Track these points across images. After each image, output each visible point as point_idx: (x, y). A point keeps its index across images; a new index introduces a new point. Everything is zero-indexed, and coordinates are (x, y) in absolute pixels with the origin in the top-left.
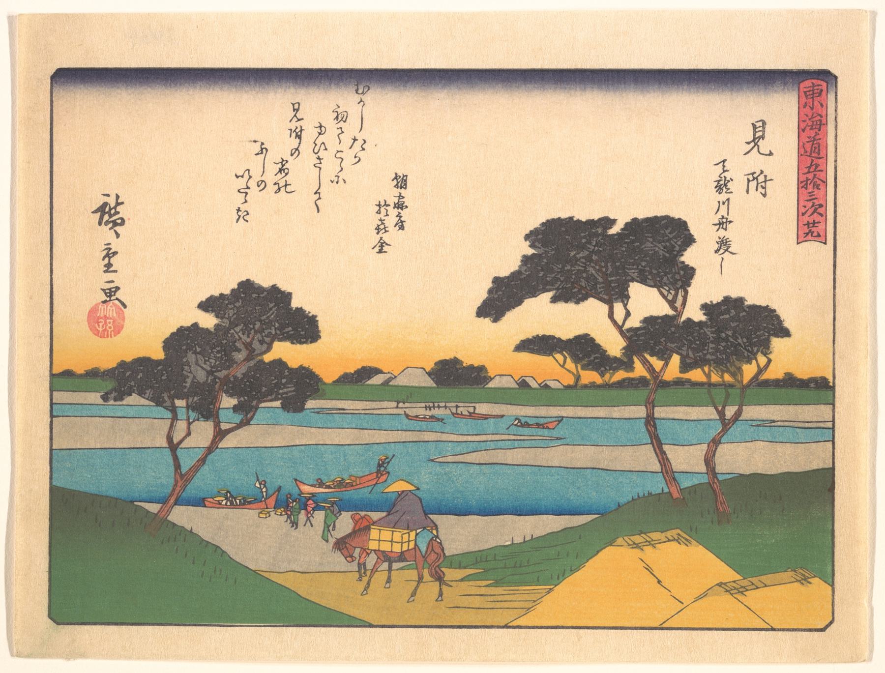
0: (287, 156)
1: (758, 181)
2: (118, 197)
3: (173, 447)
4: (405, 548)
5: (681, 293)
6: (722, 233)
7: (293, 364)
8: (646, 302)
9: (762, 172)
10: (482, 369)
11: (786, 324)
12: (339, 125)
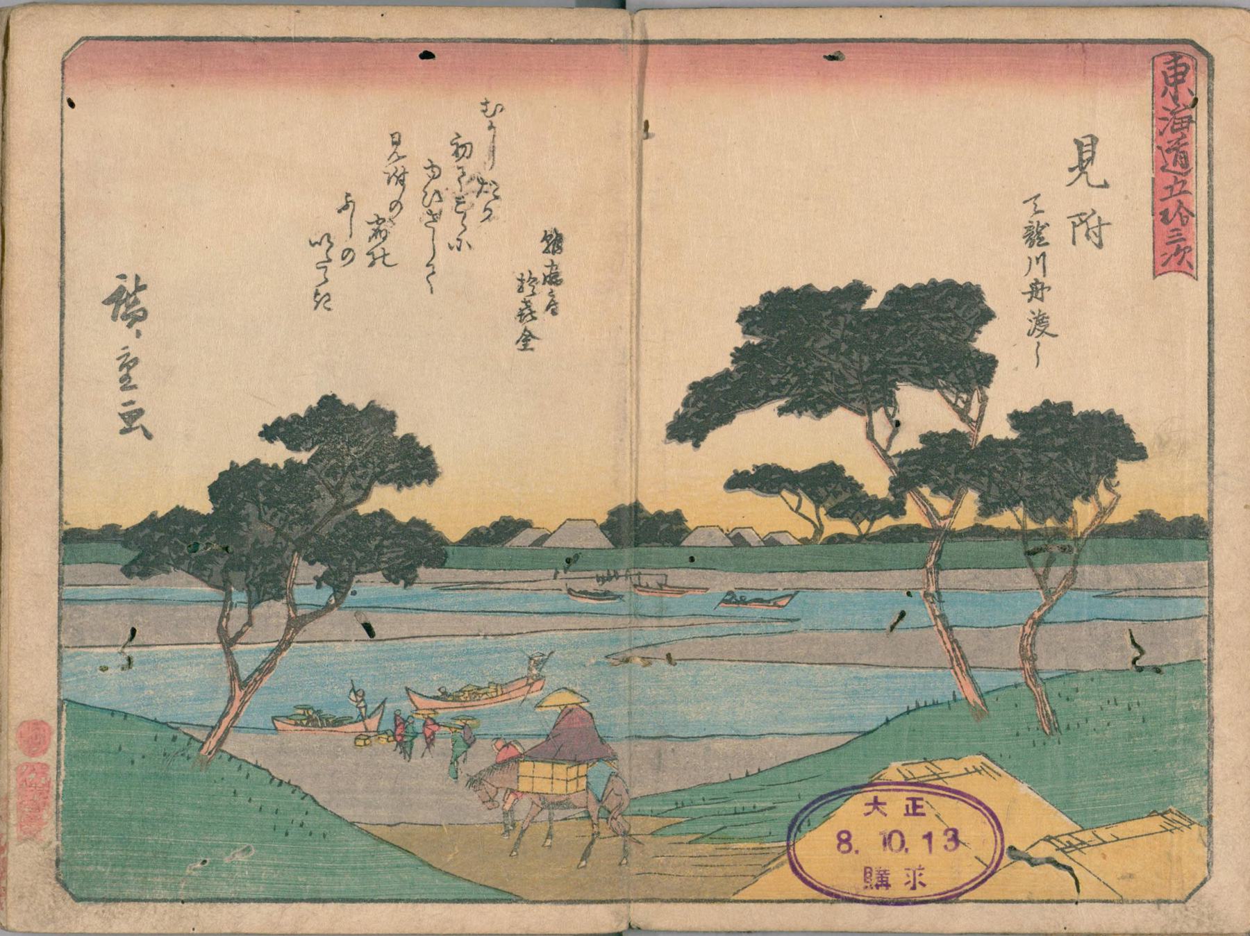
0: (385, 214)
1: (1088, 225)
2: (137, 278)
7: (403, 517)
8: (923, 410)
10: (677, 516)
11: (1138, 439)
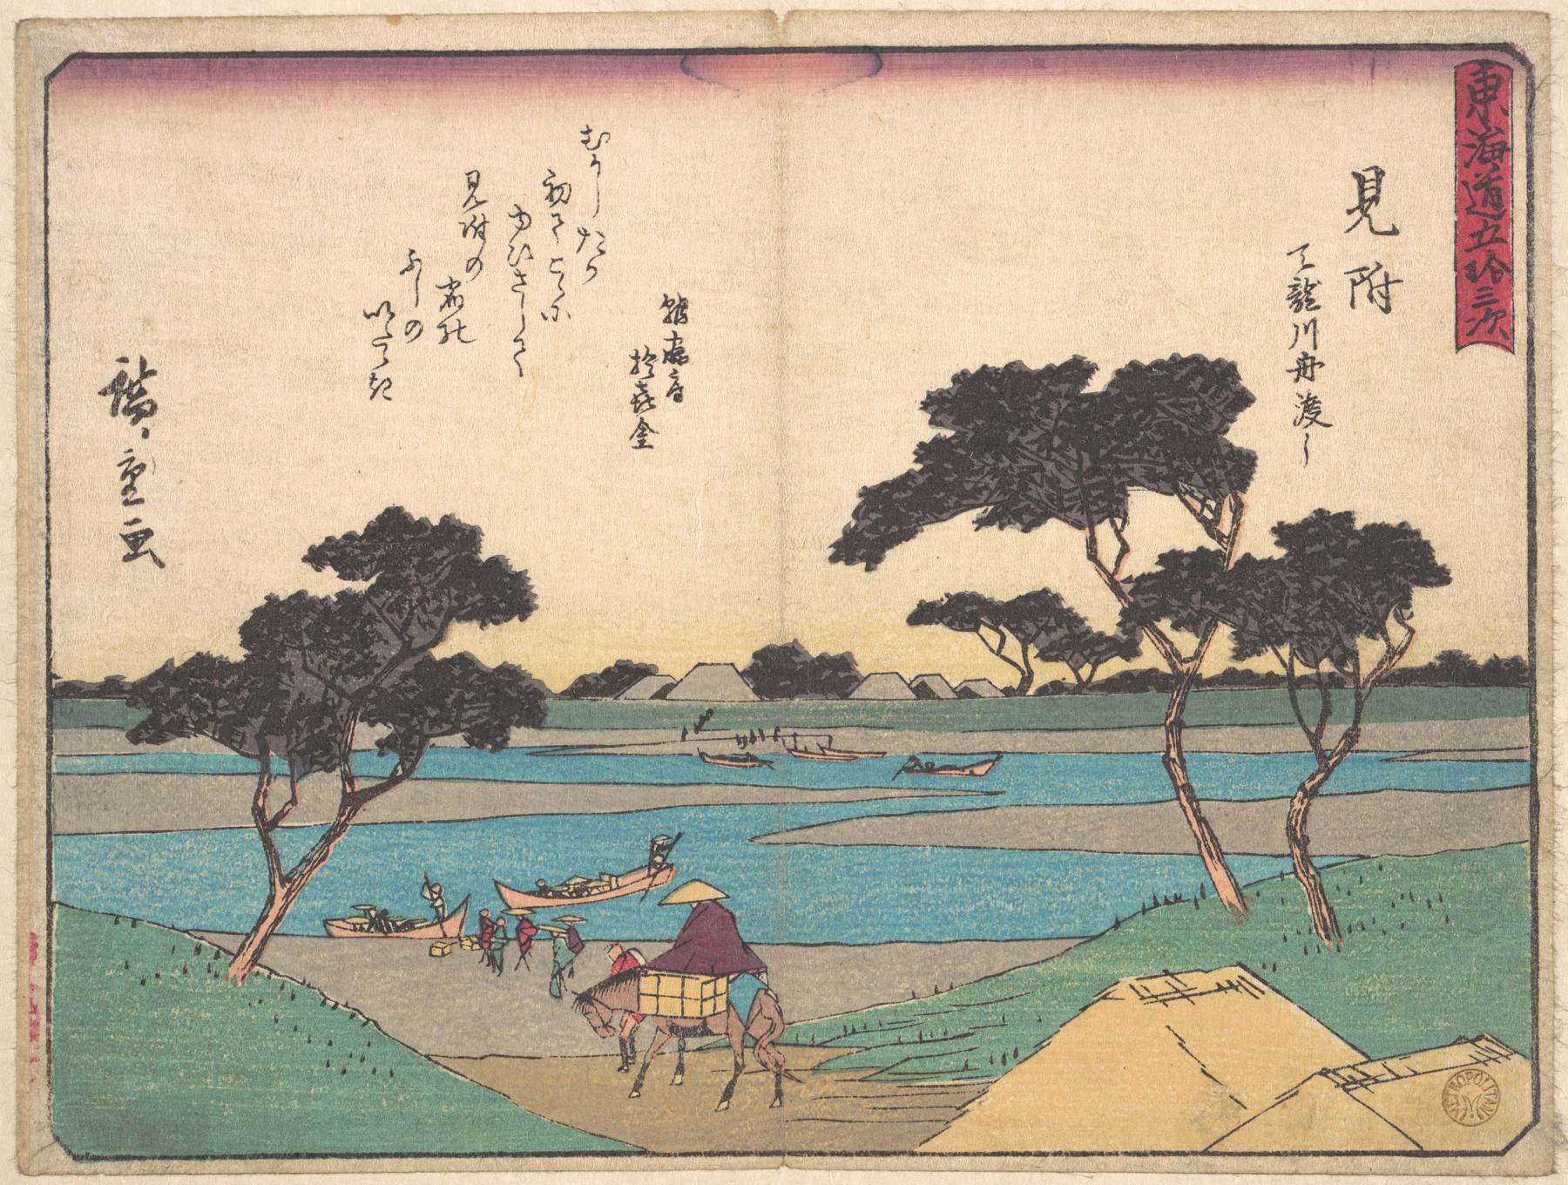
1: (1375, 285)
2: (143, 363)
3: (267, 826)
4: (708, 1008)
5: (1228, 501)
6: (1304, 386)
8: (1159, 524)
9: (1379, 267)
12: (555, 210)
